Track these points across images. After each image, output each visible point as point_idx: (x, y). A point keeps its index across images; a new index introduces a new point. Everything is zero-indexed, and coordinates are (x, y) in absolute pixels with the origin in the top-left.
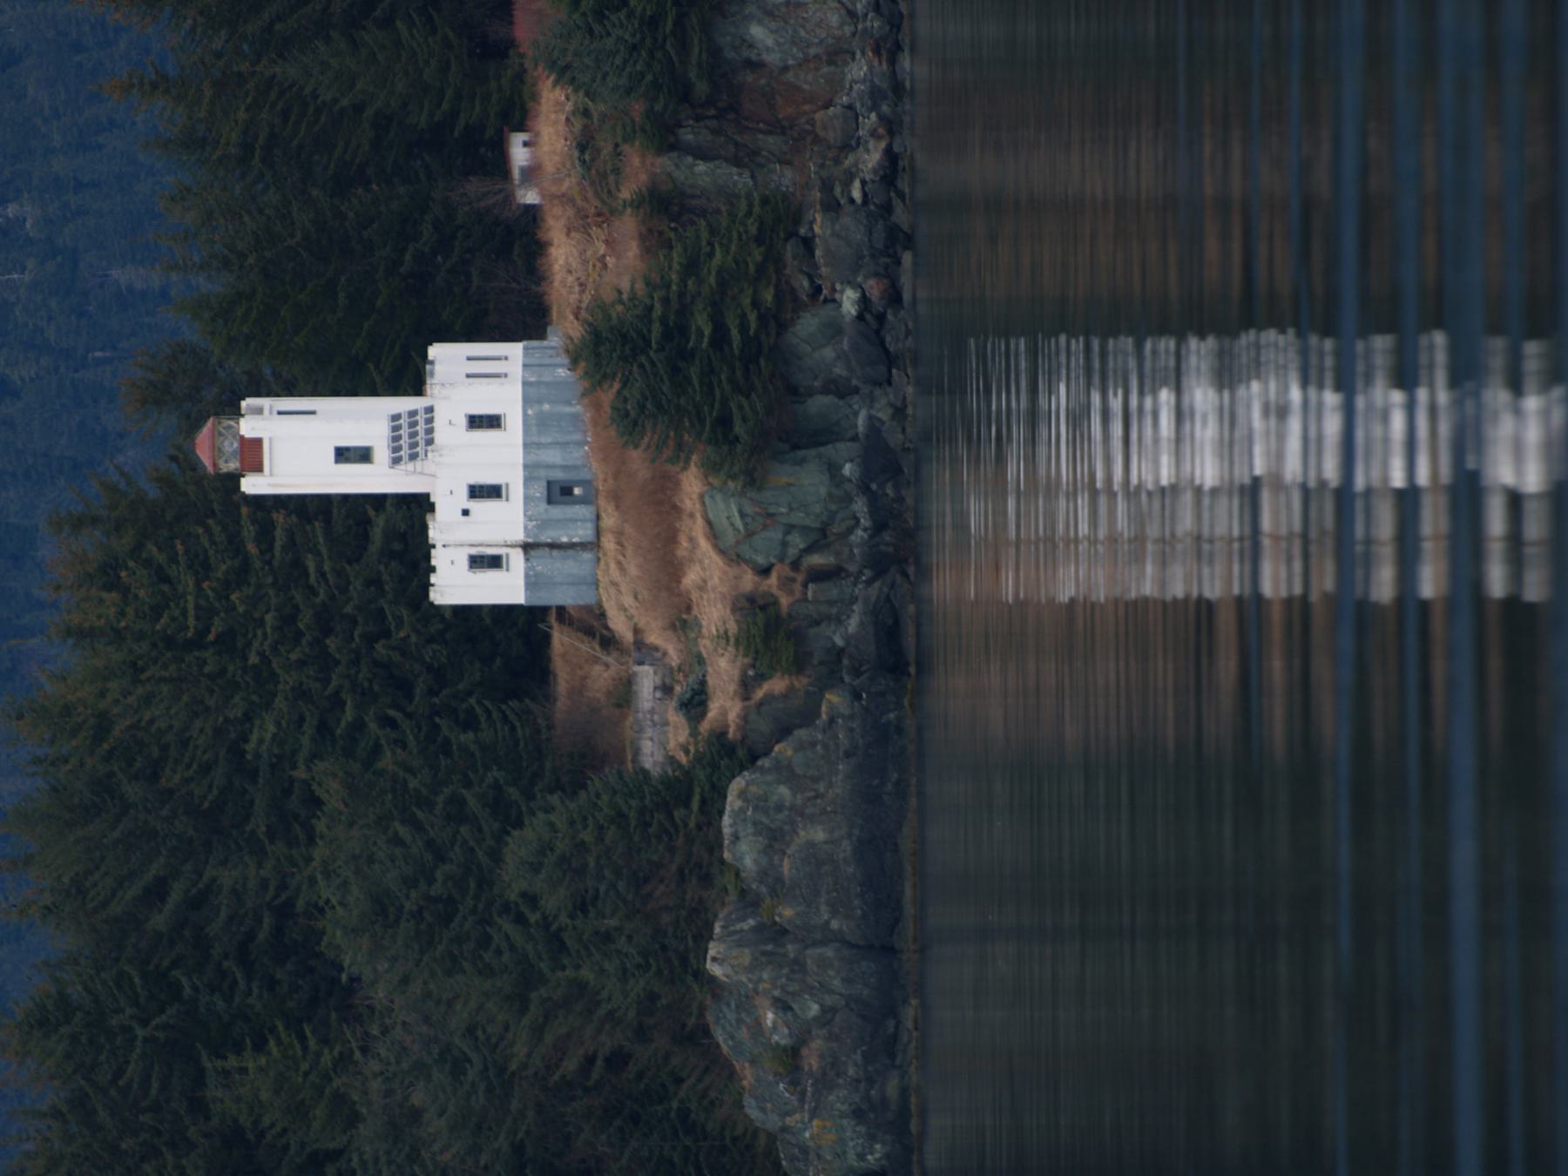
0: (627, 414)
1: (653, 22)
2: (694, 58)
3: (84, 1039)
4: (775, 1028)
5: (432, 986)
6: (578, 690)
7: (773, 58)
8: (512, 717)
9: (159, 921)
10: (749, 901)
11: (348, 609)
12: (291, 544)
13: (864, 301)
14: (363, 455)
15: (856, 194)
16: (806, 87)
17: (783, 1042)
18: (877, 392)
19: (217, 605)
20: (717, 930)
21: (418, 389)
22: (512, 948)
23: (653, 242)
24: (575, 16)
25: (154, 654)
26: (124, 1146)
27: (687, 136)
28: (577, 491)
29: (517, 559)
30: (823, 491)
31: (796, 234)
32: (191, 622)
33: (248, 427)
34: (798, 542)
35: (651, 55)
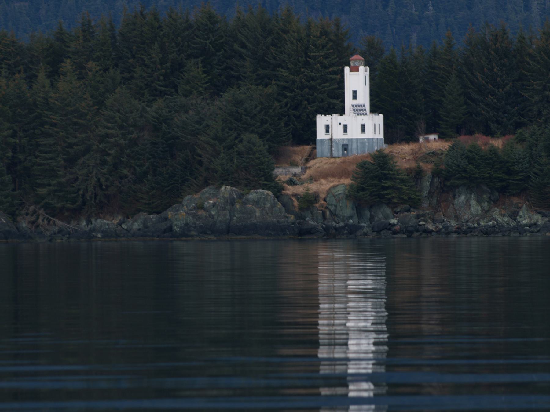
3: (206, 28)
7: (456, 201)
8: (288, 136)
9: (236, 46)
10: (241, 196)
13: (394, 225)
15: (421, 223)
18: (371, 229)
20: (233, 188)
21: (372, 111)
23: (409, 171)
26: (179, 38)
27: (436, 180)
28: (346, 152)
29: (328, 137)
30: (345, 215)
32: (312, 54)
33: (362, 68)
34: (332, 208)
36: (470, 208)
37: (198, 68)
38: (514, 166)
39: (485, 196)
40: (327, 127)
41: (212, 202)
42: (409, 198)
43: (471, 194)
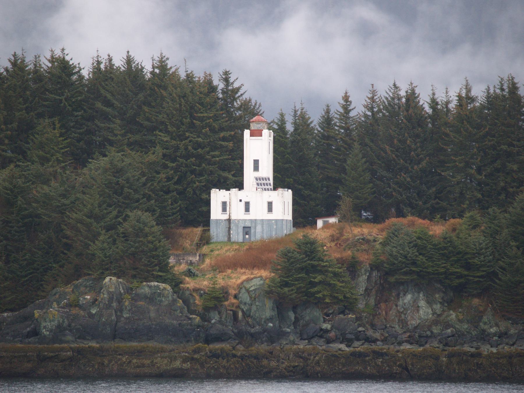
0: (289, 253)
1: (414, 263)
2: (402, 277)
3: (60, 80)
4: (85, 299)
5: (95, 187)
6: (181, 235)
7: (400, 303)
8: (175, 216)
9: (99, 105)
10: (129, 290)
11: (204, 165)
12: (222, 146)
13: (327, 331)
14: (256, 167)
16: (391, 312)
17: (80, 302)
18: (298, 335)
19: (204, 123)
20: (120, 280)
22: (108, 213)
24: (415, 238)
25: (189, 103)
27: (375, 273)
28: (247, 236)
29: (225, 217)
30: (264, 317)
31: (346, 309)
32: (199, 115)
34: (245, 308)
35: (404, 263)
36: (418, 311)
37: (54, 129)
38: (474, 258)
39: (437, 296)
40: (224, 204)
41: (89, 297)
42: (345, 297)
43: (419, 293)
